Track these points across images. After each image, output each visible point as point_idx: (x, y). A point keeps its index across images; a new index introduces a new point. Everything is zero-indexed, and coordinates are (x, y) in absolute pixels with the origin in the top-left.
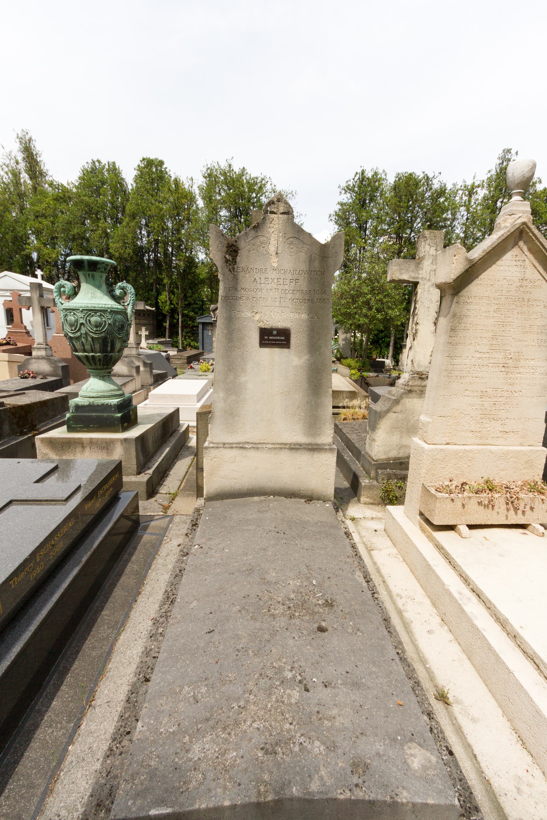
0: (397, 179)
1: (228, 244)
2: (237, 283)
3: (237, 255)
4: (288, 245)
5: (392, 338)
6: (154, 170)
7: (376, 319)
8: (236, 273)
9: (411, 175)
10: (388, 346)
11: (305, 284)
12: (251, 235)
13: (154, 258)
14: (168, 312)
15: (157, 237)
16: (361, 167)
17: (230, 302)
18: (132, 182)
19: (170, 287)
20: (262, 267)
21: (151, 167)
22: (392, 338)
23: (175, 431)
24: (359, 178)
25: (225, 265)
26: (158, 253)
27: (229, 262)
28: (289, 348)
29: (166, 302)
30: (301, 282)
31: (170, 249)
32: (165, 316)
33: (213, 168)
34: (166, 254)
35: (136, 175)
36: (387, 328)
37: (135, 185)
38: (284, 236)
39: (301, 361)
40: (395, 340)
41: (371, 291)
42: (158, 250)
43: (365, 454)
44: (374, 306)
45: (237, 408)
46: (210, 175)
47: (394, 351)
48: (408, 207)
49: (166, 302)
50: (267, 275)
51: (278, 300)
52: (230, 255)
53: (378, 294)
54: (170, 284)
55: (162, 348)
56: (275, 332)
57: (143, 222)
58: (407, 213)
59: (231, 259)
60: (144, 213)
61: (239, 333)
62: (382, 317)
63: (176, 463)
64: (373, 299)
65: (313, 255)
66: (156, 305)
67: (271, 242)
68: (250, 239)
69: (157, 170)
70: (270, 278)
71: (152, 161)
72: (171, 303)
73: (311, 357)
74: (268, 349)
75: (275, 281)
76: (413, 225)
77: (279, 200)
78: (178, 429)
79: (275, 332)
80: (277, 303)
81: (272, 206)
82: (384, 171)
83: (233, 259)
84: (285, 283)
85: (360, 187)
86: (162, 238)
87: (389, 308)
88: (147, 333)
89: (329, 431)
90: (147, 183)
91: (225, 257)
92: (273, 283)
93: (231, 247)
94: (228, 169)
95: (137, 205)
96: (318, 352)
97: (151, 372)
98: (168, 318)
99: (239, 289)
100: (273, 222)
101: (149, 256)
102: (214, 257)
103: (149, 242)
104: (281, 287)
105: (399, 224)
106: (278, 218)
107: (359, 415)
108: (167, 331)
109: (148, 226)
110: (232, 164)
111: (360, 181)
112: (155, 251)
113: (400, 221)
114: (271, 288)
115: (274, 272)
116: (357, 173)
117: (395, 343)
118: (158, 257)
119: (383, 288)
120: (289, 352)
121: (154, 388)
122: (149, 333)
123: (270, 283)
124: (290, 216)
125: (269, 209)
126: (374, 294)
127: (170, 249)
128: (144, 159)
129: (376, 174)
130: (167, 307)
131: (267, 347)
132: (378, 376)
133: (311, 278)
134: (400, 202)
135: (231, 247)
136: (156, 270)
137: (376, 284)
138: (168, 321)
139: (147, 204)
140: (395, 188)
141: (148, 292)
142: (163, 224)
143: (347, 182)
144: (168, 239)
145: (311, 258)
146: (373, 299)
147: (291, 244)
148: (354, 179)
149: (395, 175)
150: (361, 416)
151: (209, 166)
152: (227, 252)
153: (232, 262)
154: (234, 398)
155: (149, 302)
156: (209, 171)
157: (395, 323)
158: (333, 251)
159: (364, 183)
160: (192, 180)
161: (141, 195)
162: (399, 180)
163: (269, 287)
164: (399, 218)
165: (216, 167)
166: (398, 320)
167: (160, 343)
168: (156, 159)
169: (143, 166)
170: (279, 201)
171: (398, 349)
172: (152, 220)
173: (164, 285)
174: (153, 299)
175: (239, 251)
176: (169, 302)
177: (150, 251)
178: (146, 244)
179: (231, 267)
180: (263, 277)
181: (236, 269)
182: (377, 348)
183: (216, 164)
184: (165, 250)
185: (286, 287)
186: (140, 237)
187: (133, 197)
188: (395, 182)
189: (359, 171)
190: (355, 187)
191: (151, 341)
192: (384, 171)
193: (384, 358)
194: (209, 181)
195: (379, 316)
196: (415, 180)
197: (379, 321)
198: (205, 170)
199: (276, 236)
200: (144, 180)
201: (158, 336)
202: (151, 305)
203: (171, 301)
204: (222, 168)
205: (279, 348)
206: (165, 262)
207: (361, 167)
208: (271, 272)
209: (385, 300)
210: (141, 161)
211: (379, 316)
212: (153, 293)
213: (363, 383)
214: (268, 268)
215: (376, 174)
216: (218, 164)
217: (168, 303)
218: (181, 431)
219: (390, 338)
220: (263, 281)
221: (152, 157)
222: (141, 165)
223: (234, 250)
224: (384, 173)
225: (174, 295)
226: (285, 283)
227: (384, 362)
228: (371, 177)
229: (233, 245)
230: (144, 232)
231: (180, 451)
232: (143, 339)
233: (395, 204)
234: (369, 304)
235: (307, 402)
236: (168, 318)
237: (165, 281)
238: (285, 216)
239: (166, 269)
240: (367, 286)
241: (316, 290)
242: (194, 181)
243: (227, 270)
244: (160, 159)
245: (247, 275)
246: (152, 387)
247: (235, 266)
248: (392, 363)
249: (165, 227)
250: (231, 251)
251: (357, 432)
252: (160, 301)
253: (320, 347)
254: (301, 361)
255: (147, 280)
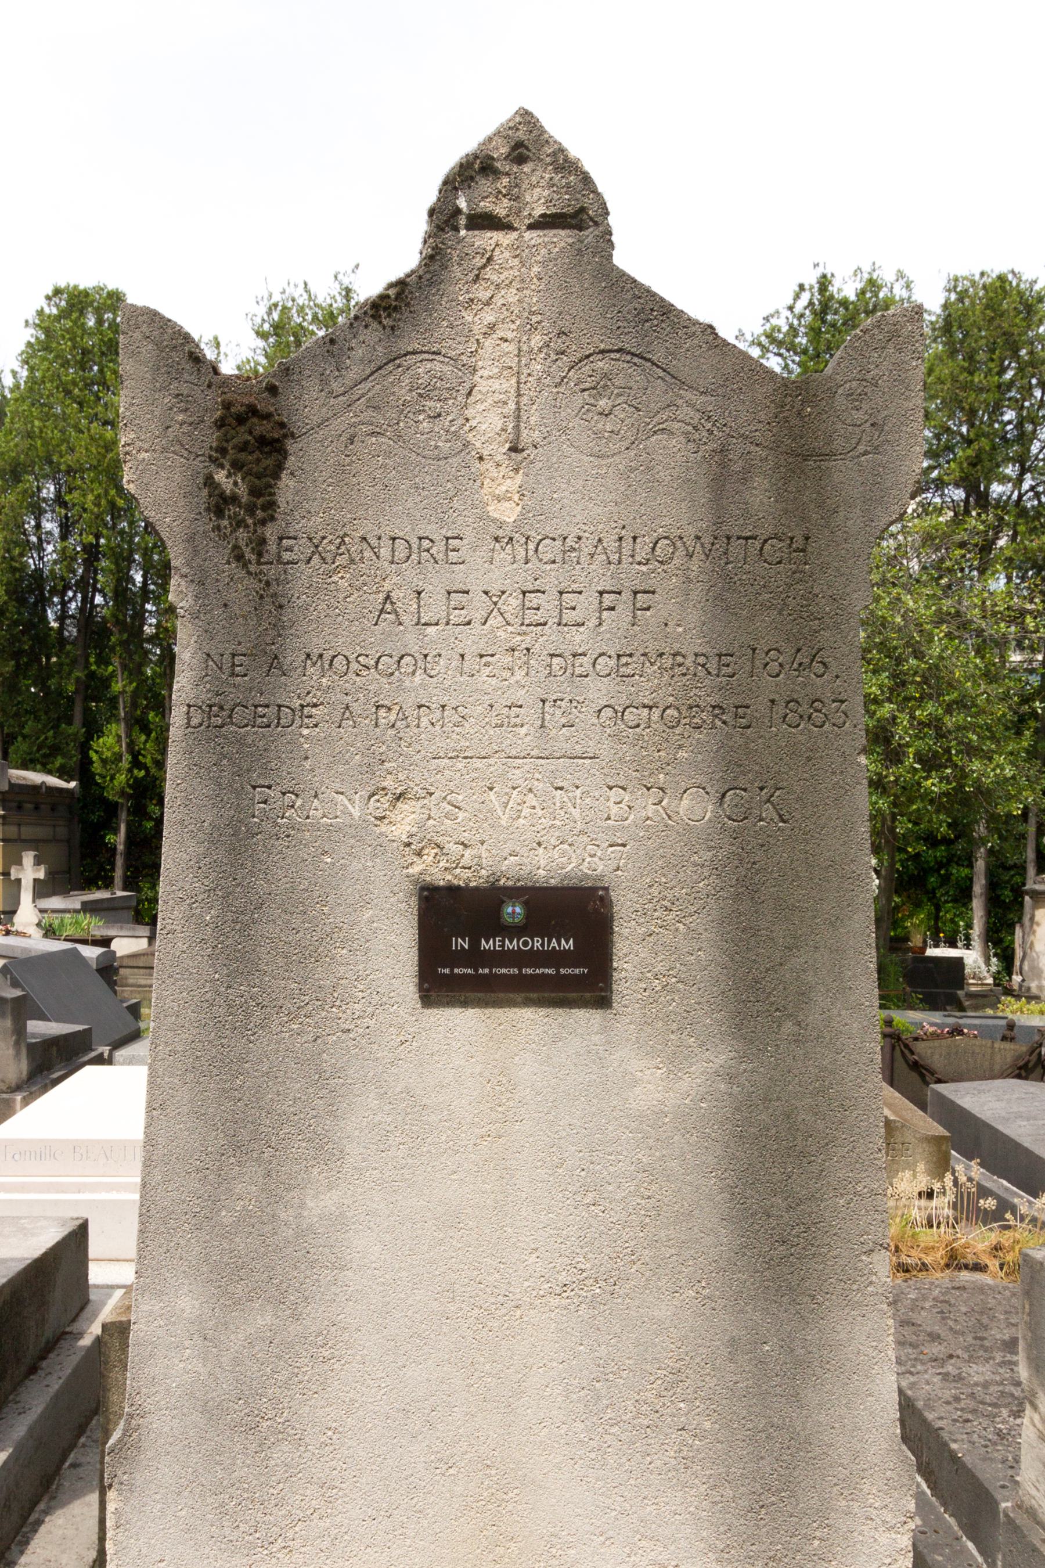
0: (953, 297)
1: (227, 406)
2: (279, 628)
3: (280, 467)
4: (579, 400)
5: (980, 865)
6: (91, 322)
7: (922, 797)
8: (272, 571)
9: (1002, 278)
10: (964, 895)
11: (694, 616)
12: (359, 352)
13: (81, 609)
14: (122, 793)
15: (91, 539)
16: (816, 265)
17: (240, 741)
18: (16, 366)
19: (134, 705)
20: (429, 530)
21: (82, 313)
22: (980, 865)
23: (63, 1336)
24: (811, 303)
25: (205, 525)
26: (95, 590)
27: (233, 509)
28: (603, 1002)
29: (118, 757)
30: (664, 606)
31: (138, 578)
32: (112, 809)
33: (290, 304)
34: (121, 593)
35: (29, 344)
36: (961, 830)
37: (24, 373)
38: (558, 344)
39: (684, 1084)
40: (990, 874)
41: (891, 690)
42: (96, 581)
43: (1021, 1519)
44: (908, 745)
45: (286, 1385)
46: (278, 328)
47: (988, 913)
48: (1003, 388)
49: (118, 757)
50: (459, 577)
51: (530, 714)
52: (237, 466)
53: (922, 698)
54: (135, 694)
55: (95, 926)
56: (514, 911)
57: (49, 490)
58: (996, 409)
59: (242, 491)
60: (50, 462)
61: (296, 921)
62: (944, 787)
63: (39, 1522)
64: (904, 719)
65: (738, 447)
66: (83, 771)
67: (483, 386)
68: (353, 373)
69: (100, 322)
70: (476, 589)
71: (86, 293)
72: (136, 763)
73: (742, 1057)
74: (471, 1012)
75: (513, 602)
76: (1029, 450)
77: (519, 153)
78: (75, 1328)
79: (514, 911)
80: (525, 738)
81: (484, 185)
82: (900, 275)
83: (254, 492)
84: (569, 616)
85: (815, 333)
86: (109, 540)
87: (971, 751)
88: (41, 875)
89: (884, 1538)
90: (66, 364)
91: (209, 481)
92: (495, 621)
93: (241, 420)
94: (340, 303)
95: (30, 435)
96: (788, 1027)
97: (20, 1031)
98: (123, 815)
99: (292, 658)
100: (488, 273)
101: (64, 604)
102: (146, 487)
103: (66, 557)
104: (550, 638)
105: (975, 446)
106: (516, 250)
107: (927, 1250)
108: (119, 861)
109: (64, 504)
110: (354, 287)
111: (814, 313)
112: (86, 586)
113: (978, 436)
114: (482, 647)
115: (503, 556)
116: (802, 287)
117: (993, 885)
118: (94, 606)
119: (938, 678)
120: (604, 1030)
121: (26, 1102)
122: (50, 873)
123: (478, 616)
124: (590, 234)
125: (462, 203)
126: (907, 699)
127: (138, 578)
128: (57, 292)
129: (873, 284)
130: (122, 778)
131: (465, 1004)
132: (957, 1031)
133: (728, 579)
134: (971, 373)
135: (241, 420)
136: (86, 647)
137: (912, 661)
138: (123, 828)
139: (63, 431)
140: (948, 326)
141: (56, 727)
142: (113, 492)
143: (767, 319)
144: (131, 542)
145: (723, 465)
146: (904, 719)
147: (597, 390)
148: (791, 308)
149: (943, 283)
150: (939, 1256)
151: (277, 298)
152: (218, 455)
153: (251, 510)
154: (263, 1319)
155: (59, 761)
156: (276, 316)
157: (1001, 810)
158: (858, 416)
159: (829, 317)
160: (218, 345)
161: (43, 405)
162: (961, 300)
163: (471, 641)
164: (972, 425)
165: (300, 302)
166: (1009, 798)
167: (89, 908)
168: (99, 289)
169: (55, 311)
170: (521, 160)
171: (1006, 907)
172: (79, 482)
173: (113, 702)
174: (73, 749)
175: (291, 446)
176: (127, 758)
177: (67, 587)
178: (55, 562)
179: (242, 534)
180: (435, 583)
181: (272, 547)
182: (918, 905)
183: (301, 289)
184: (119, 581)
185: (579, 638)
186: (34, 539)
187: (15, 413)
188: (945, 306)
189: (811, 279)
190: (796, 336)
191: (55, 902)
192: (900, 275)
193: (953, 944)
194: (278, 344)
195: (932, 784)
196: (1020, 294)
197: (932, 801)
198: (261, 311)
199: (511, 348)
200: (57, 357)
201: (88, 883)
202: (63, 773)
203: (135, 755)
204: (319, 301)
205: (540, 1003)
206: (118, 622)
207: (816, 265)
208: (483, 553)
209: (949, 722)
210: (48, 298)
211: (932, 784)
212: (72, 730)
213: (900, 1064)
214: (468, 533)
215: (873, 284)
216: (307, 290)
217: (125, 763)
218: (86, 1341)
219: (971, 866)
220: (435, 607)
221: (86, 282)
222: (47, 311)
223: (263, 442)
224: (902, 282)
225: (148, 735)
226: (569, 616)
227: (959, 962)
228: (852, 298)
229: (253, 410)
230: (50, 525)
231: (72, 1446)
232: (26, 896)
233: (954, 380)
234: (887, 741)
235: (733, 1342)
236: (123, 815)
237: (117, 686)
238: (561, 238)
239: (122, 643)
240: (875, 672)
241: (762, 646)
242: (222, 349)
243: (219, 557)
244: (111, 287)
245: (342, 581)
246: (19, 1098)
247: (270, 532)
248: (987, 963)
249: (121, 503)
250: (244, 448)
251: (935, 1349)
252: (94, 757)
253: (804, 995)
254: (684, 1084)
255: (52, 683)
